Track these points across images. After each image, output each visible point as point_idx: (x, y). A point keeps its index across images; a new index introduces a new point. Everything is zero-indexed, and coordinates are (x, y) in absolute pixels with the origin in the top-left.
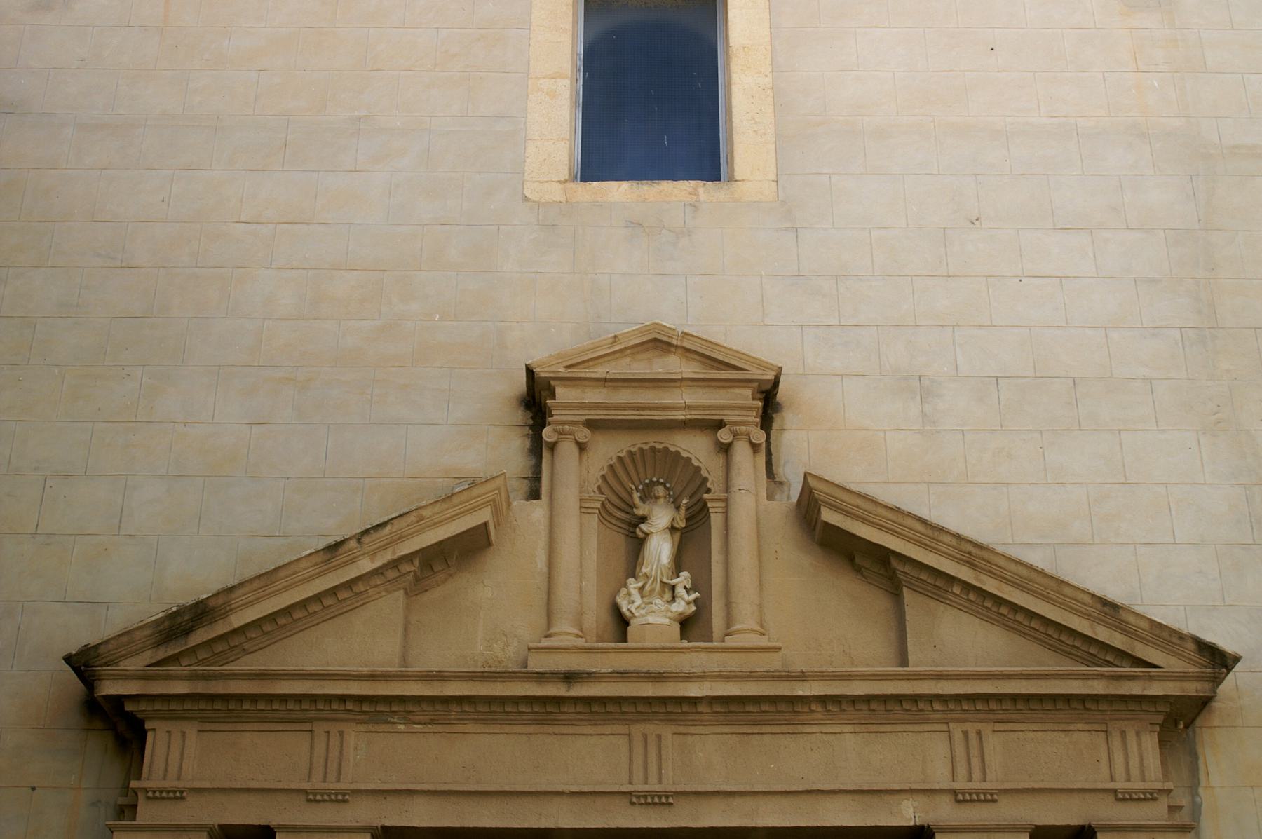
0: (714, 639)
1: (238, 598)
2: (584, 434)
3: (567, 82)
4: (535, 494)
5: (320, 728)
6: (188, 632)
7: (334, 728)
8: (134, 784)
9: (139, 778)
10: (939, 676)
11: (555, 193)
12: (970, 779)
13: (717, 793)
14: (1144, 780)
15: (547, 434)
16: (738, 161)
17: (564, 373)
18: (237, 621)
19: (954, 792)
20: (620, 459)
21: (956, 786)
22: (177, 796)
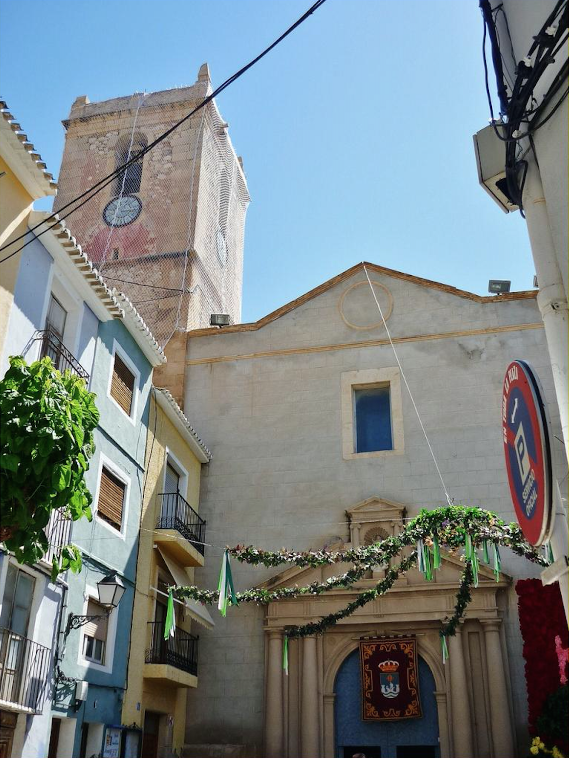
0: (430, 744)
1: (285, 574)
2: (360, 526)
3: (352, 425)
4: (349, 541)
5: (305, 602)
6: (274, 582)
7: (309, 602)
8: (267, 617)
9: (267, 615)
10: (522, 466)
11: (350, 457)
12: (450, 608)
13: (393, 614)
14: (488, 607)
15: (351, 527)
16: (395, 446)
17: (354, 511)
18: (285, 579)
19: (447, 611)
20: (369, 531)
21: (447, 610)
22: (276, 619)
